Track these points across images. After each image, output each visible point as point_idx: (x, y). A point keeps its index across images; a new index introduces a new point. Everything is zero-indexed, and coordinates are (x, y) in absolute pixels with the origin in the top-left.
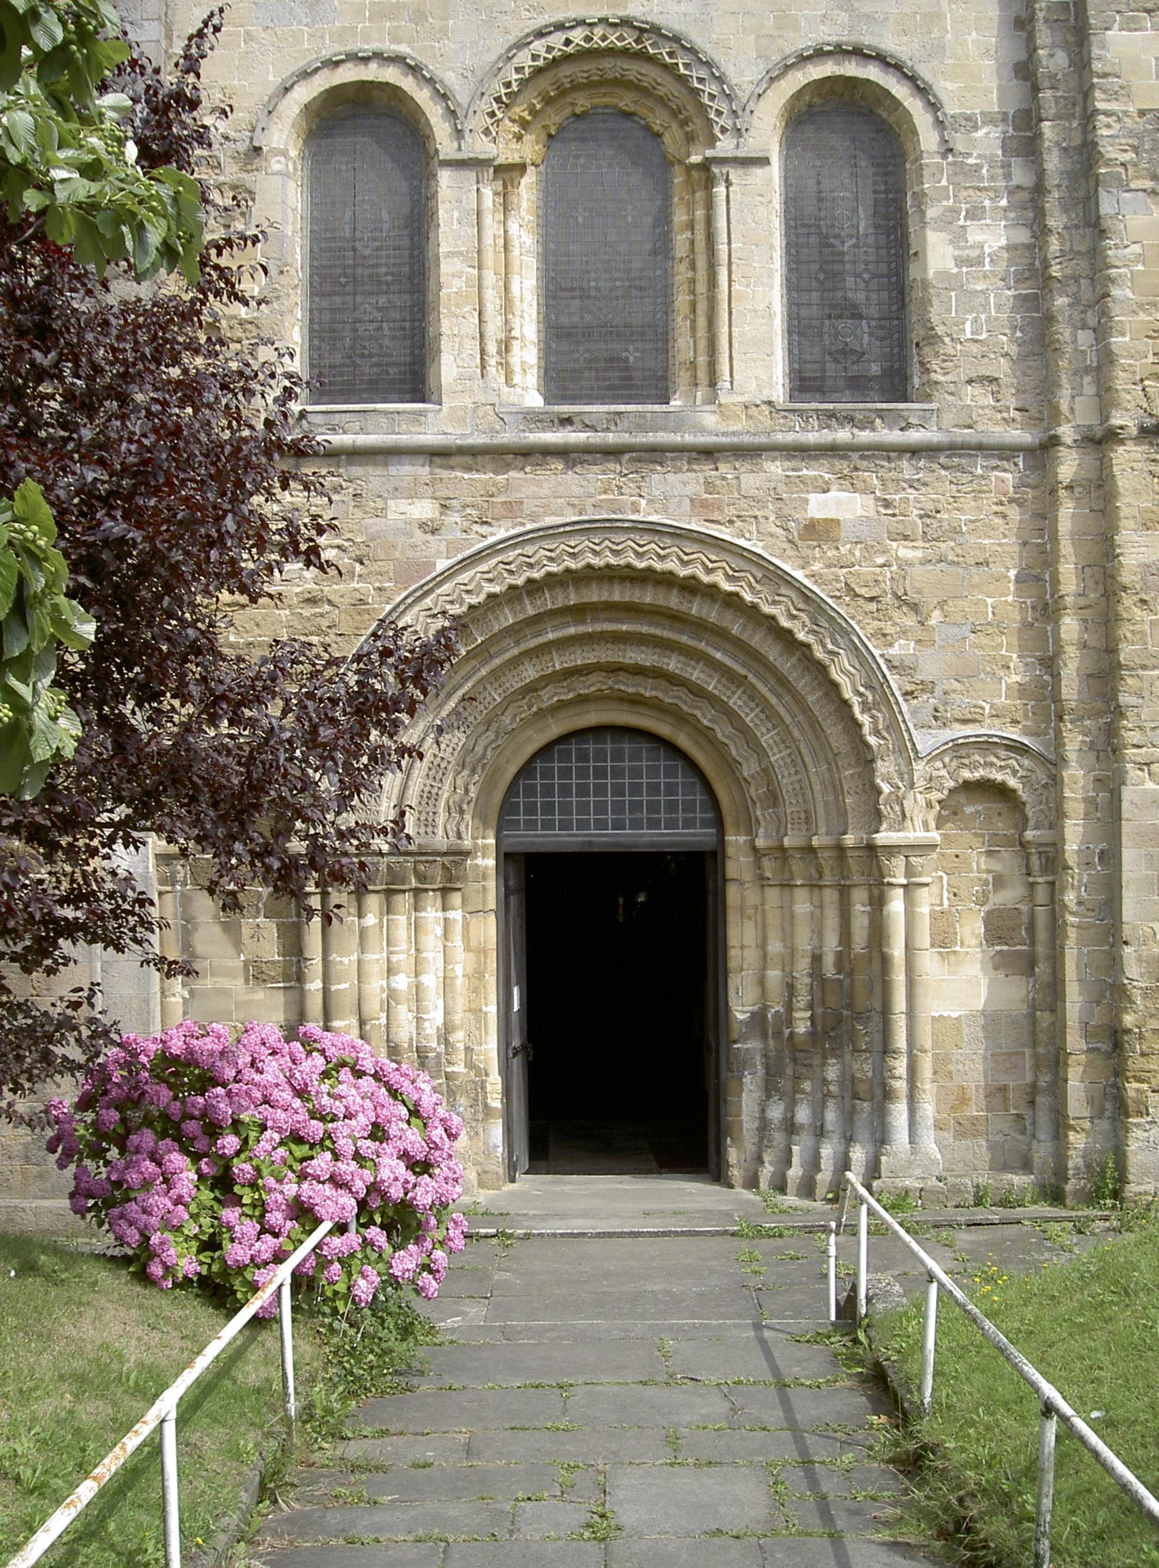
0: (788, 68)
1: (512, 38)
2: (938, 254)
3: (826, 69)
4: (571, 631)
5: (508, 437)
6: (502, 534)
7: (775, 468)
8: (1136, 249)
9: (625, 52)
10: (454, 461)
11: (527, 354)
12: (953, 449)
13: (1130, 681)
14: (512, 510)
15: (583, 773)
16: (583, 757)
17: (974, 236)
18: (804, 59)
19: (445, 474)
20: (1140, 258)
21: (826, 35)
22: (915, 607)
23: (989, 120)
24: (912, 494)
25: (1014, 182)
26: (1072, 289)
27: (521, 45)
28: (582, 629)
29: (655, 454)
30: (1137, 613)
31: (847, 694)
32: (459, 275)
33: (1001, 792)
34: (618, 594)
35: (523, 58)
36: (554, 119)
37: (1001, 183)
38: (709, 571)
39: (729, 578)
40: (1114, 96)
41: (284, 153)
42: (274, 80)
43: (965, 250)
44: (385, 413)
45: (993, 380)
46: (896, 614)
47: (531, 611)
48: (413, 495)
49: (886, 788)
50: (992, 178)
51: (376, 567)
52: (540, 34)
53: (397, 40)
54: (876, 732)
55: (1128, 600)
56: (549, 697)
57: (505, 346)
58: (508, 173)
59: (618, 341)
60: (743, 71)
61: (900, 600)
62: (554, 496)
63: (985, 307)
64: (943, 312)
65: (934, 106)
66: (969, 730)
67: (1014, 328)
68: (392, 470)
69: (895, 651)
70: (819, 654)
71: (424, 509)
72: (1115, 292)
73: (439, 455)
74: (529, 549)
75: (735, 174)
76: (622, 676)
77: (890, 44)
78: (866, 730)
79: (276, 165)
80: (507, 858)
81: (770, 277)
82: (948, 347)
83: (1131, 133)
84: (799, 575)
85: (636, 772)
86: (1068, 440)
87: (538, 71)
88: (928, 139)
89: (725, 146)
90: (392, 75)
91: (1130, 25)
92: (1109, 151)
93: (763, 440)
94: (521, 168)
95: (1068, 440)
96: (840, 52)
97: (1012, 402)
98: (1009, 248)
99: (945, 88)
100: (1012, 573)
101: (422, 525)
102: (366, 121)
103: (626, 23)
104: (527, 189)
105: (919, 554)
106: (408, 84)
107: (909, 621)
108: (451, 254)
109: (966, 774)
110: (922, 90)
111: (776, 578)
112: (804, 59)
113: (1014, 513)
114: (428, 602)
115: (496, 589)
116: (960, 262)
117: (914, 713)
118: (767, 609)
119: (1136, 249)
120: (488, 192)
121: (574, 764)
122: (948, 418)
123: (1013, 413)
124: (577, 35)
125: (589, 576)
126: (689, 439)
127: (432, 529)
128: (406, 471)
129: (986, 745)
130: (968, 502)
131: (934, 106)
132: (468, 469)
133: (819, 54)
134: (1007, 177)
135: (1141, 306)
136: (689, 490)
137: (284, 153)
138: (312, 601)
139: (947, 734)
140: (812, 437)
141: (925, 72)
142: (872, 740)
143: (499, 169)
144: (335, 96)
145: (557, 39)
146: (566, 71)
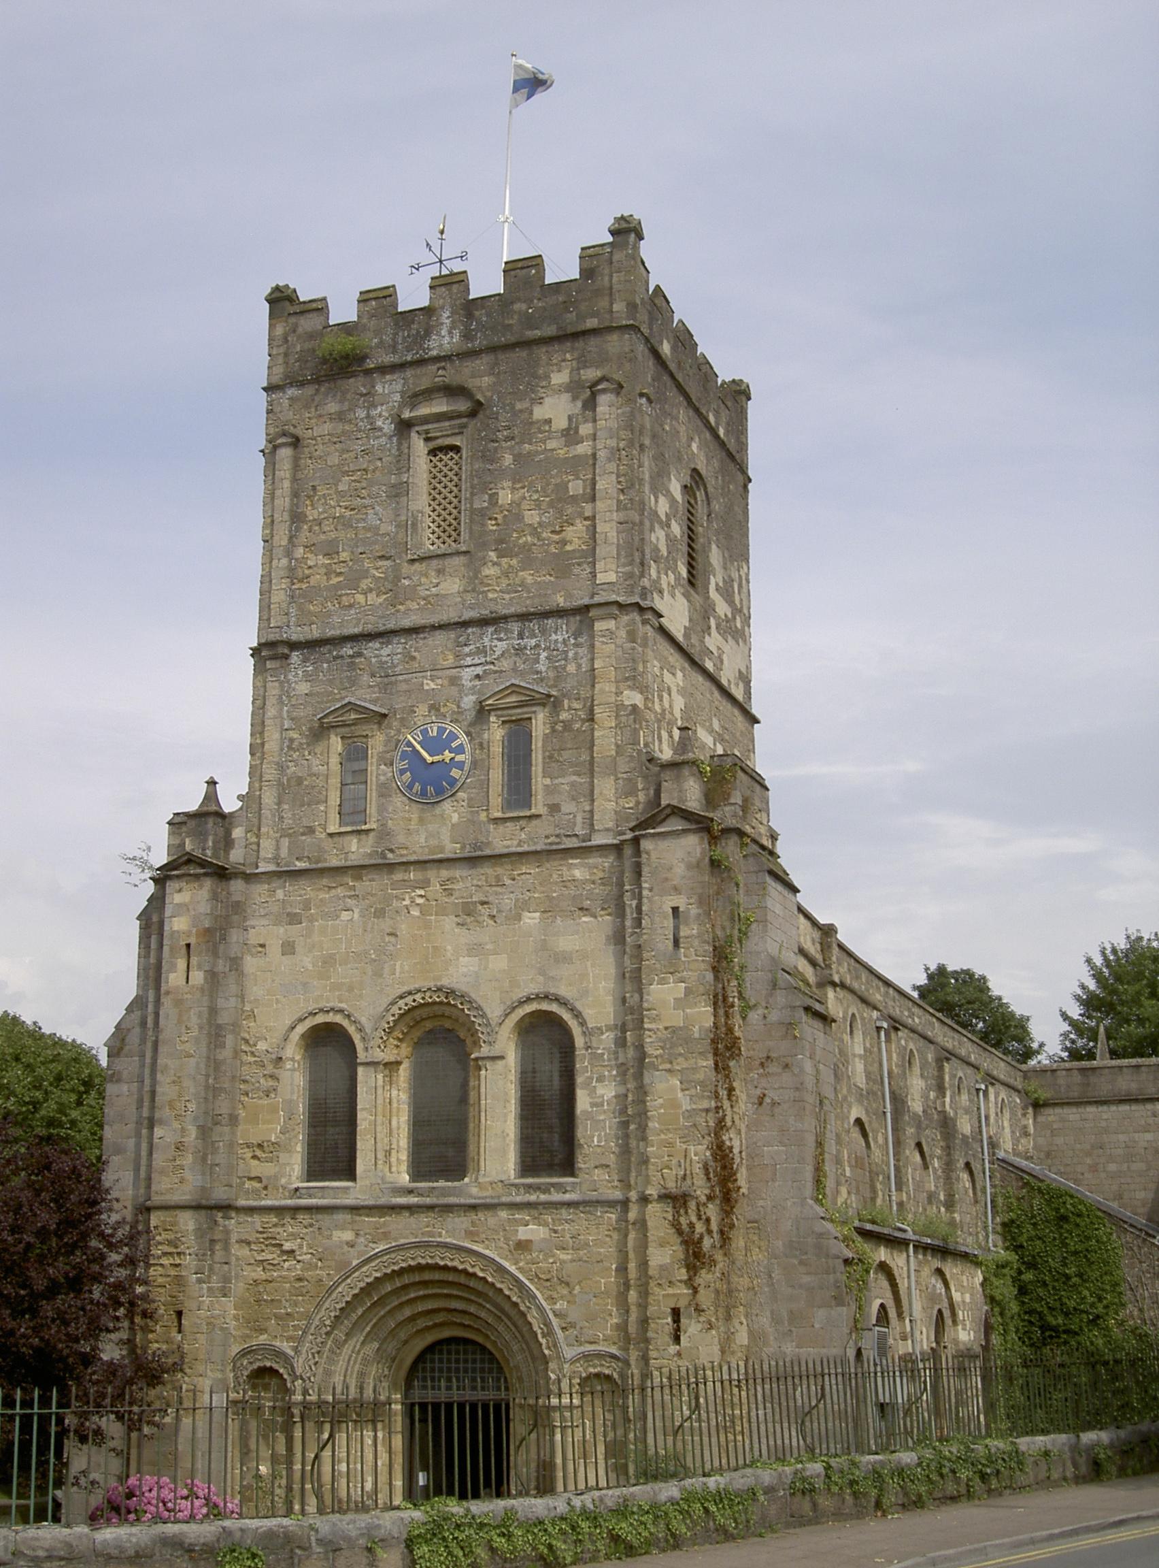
0: (514, 1008)
1: (390, 999)
2: (583, 1102)
3: (529, 1008)
4: (421, 1293)
5: (383, 1201)
6: (382, 1247)
7: (503, 1214)
8: (661, 1101)
9: (441, 1003)
10: (361, 1212)
11: (402, 1156)
12: (585, 1203)
13: (652, 1325)
14: (386, 1236)
15: (457, 1361)
16: (449, 1352)
17: (600, 1091)
18: (521, 1003)
19: (358, 1218)
20: (662, 1106)
21: (533, 988)
22: (567, 1284)
23: (609, 1028)
24: (567, 1226)
25: (620, 1061)
26: (638, 1120)
27: (393, 1003)
28: (426, 1292)
29: (448, 1208)
30: (657, 1290)
31: (536, 1328)
32: (365, 1119)
33: (608, 1378)
34: (437, 1276)
35: (395, 1010)
36: (417, 1034)
37: (613, 1063)
38: (473, 1266)
39: (482, 1270)
40: (653, 1020)
41: (293, 1059)
42: (288, 1022)
43: (597, 1097)
44: (332, 1188)
45: (608, 1166)
46: (559, 1288)
47: (398, 1285)
48: (343, 1229)
49: (553, 1376)
50: (609, 1060)
51: (327, 1263)
52: (401, 997)
53: (341, 1001)
54: (549, 1348)
55: (652, 1284)
56: (422, 1323)
57: (388, 1153)
58: (392, 1066)
59: (442, 1147)
60: (494, 1011)
61: (561, 1281)
62: (406, 1229)
63: (604, 1128)
64: (583, 1132)
65: (583, 1024)
66: (592, 1347)
67: (618, 1139)
68: (335, 1217)
69: (558, 1306)
70: (523, 1308)
71: (348, 1236)
72: (650, 1124)
73: (355, 1209)
74: (393, 1256)
75: (489, 1064)
76: (455, 1314)
77: (563, 991)
78: (544, 1346)
79: (289, 1065)
80: (409, 1409)
81: (505, 1115)
82: (586, 1150)
83: (660, 1040)
84: (512, 1269)
85: (474, 1361)
86: (634, 1200)
87: (401, 1016)
88: (579, 1041)
89: (485, 1051)
90: (338, 1019)
91: (662, 982)
92: (649, 1050)
93: (496, 1201)
94: (399, 1063)
95: (634, 1200)
96: (538, 998)
97: (616, 1177)
98: (615, 1097)
99: (588, 1013)
100: (614, 1266)
101: (347, 1243)
102: (329, 1041)
103: (439, 989)
104: (404, 1072)
105: (569, 1257)
106: (345, 1023)
107: (565, 1292)
108: (363, 1109)
109: (592, 1370)
110: (578, 1015)
111: (501, 1270)
112: (521, 1003)
113: (615, 1236)
114: (349, 1281)
115: (378, 1275)
116: (593, 1105)
117: (566, 1338)
118: (499, 1285)
119: (661, 1101)
120: (380, 1076)
121: (445, 1356)
122: (585, 1187)
123: (616, 1183)
124: (418, 997)
125: (420, 1268)
126: (462, 1201)
127: (351, 1245)
128: (340, 1217)
129: (600, 1356)
130: (593, 1229)
131: (583, 1024)
132: (368, 1216)
133: (529, 1000)
134: (617, 1059)
135: (662, 1131)
136: (464, 1226)
137: (293, 1059)
138: (300, 1280)
139: (582, 1349)
140: (518, 1199)
141: (578, 1006)
142: (546, 1352)
143: (386, 1065)
144: (316, 1029)
145: (409, 999)
146: (417, 1013)
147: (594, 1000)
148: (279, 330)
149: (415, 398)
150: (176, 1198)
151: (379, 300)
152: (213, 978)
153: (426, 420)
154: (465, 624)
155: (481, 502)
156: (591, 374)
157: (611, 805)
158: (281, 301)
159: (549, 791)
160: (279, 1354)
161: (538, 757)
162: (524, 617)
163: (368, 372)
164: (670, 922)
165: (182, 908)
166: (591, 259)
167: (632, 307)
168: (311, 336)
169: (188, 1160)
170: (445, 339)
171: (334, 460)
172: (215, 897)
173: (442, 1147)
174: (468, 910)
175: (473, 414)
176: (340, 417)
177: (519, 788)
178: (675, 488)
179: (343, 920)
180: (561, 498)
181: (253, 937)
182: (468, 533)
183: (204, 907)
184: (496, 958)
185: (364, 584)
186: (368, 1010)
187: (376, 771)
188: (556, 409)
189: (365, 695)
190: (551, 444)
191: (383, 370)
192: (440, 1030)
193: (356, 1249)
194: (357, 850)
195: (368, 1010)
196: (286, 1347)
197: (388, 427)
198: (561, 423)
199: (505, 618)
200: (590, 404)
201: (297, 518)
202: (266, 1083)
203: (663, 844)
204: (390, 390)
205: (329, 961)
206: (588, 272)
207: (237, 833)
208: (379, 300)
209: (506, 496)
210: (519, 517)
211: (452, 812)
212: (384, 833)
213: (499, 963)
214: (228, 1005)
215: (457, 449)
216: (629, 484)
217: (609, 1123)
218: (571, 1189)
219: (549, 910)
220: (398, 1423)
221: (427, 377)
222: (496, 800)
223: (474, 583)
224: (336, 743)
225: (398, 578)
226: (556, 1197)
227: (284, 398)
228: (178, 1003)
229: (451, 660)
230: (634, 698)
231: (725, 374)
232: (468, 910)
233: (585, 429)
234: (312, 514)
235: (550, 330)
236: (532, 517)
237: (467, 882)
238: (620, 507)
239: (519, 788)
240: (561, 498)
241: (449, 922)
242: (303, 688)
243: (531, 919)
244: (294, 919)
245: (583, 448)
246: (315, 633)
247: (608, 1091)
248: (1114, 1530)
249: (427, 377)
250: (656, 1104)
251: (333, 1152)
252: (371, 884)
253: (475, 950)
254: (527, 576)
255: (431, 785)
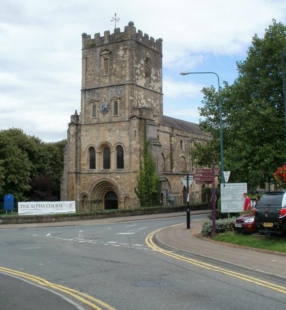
29: (107, 173)
59: (107, 165)
60: (113, 145)
62: (102, 176)
77: (122, 142)
104: (102, 153)
147: (126, 143)
148: (84, 40)
149: (102, 51)
150: (72, 172)
151: (97, 35)
152: (76, 140)
153: (104, 55)
154: (109, 87)
155: (111, 68)
156: (126, 47)
157: (127, 114)
158: (84, 35)
159: (120, 112)
160: (86, 193)
161: (118, 107)
162: (117, 85)
163: (96, 47)
164: (134, 133)
165: (72, 130)
166: (126, 28)
167: (132, 36)
168: (88, 41)
169: (74, 166)
170: (106, 42)
171: (91, 61)
172: (76, 128)
173: (107, 165)
174: (109, 130)
175: (110, 54)
176: (92, 54)
177: (116, 112)
178: (142, 62)
179: (93, 131)
180: (122, 67)
181: (82, 134)
182: (111, 73)
183: (75, 130)
184: (113, 137)
185: (96, 80)
186: (96, 145)
187: (97, 109)
188: (121, 53)
189: (96, 98)
190: (120, 58)
191: (98, 46)
192: (106, 148)
193: (96, 179)
194: (95, 121)
195: (96, 145)
196: (88, 192)
197: (99, 56)
198: (122, 55)
199: (114, 86)
200: (126, 52)
201: (86, 70)
202: (84, 155)
203: (134, 121)
204: (99, 50)
205: (91, 137)
206: (125, 31)
207: (80, 118)
208: (97, 35)
209: (114, 67)
210: (116, 70)
211: (107, 115)
212: (99, 119)
213: (113, 138)
214: (78, 144)
215: (108, 59)
216: (131, 64)
217: (128, 161)
218: (123, 170)
219: (120, 130)
220: (104, 203)
221: (104, 48)
222: (113, 114)
223: (110, 80)
224: (92, 105)
225: (100, 79)
226: (121, 172)
227: (84, 51)
228: (72, 144)
229: (107, 92)
230: (131, 98)
231: (156, 38)
232: (109, 130)
233: (125, 56)
234: (89, 69)
235: (120, 40)
236: (118, 70)
237: (109, 126)
238: (130, 68)
239: (116, 112)
240: (122, 67)
241: (107, 132)
242: (88, 96)
243: (118, 131)
244: (87, 131)
245: (124, 59)
246: (89, 88)
247: (128, 156)
248: (68, 220)
249: (104, 48)
250: (133, 158)
251: (93, 165)
252: (97, 126)
253: (110, 136)
254: (117, 79)
255: (105, 111)
